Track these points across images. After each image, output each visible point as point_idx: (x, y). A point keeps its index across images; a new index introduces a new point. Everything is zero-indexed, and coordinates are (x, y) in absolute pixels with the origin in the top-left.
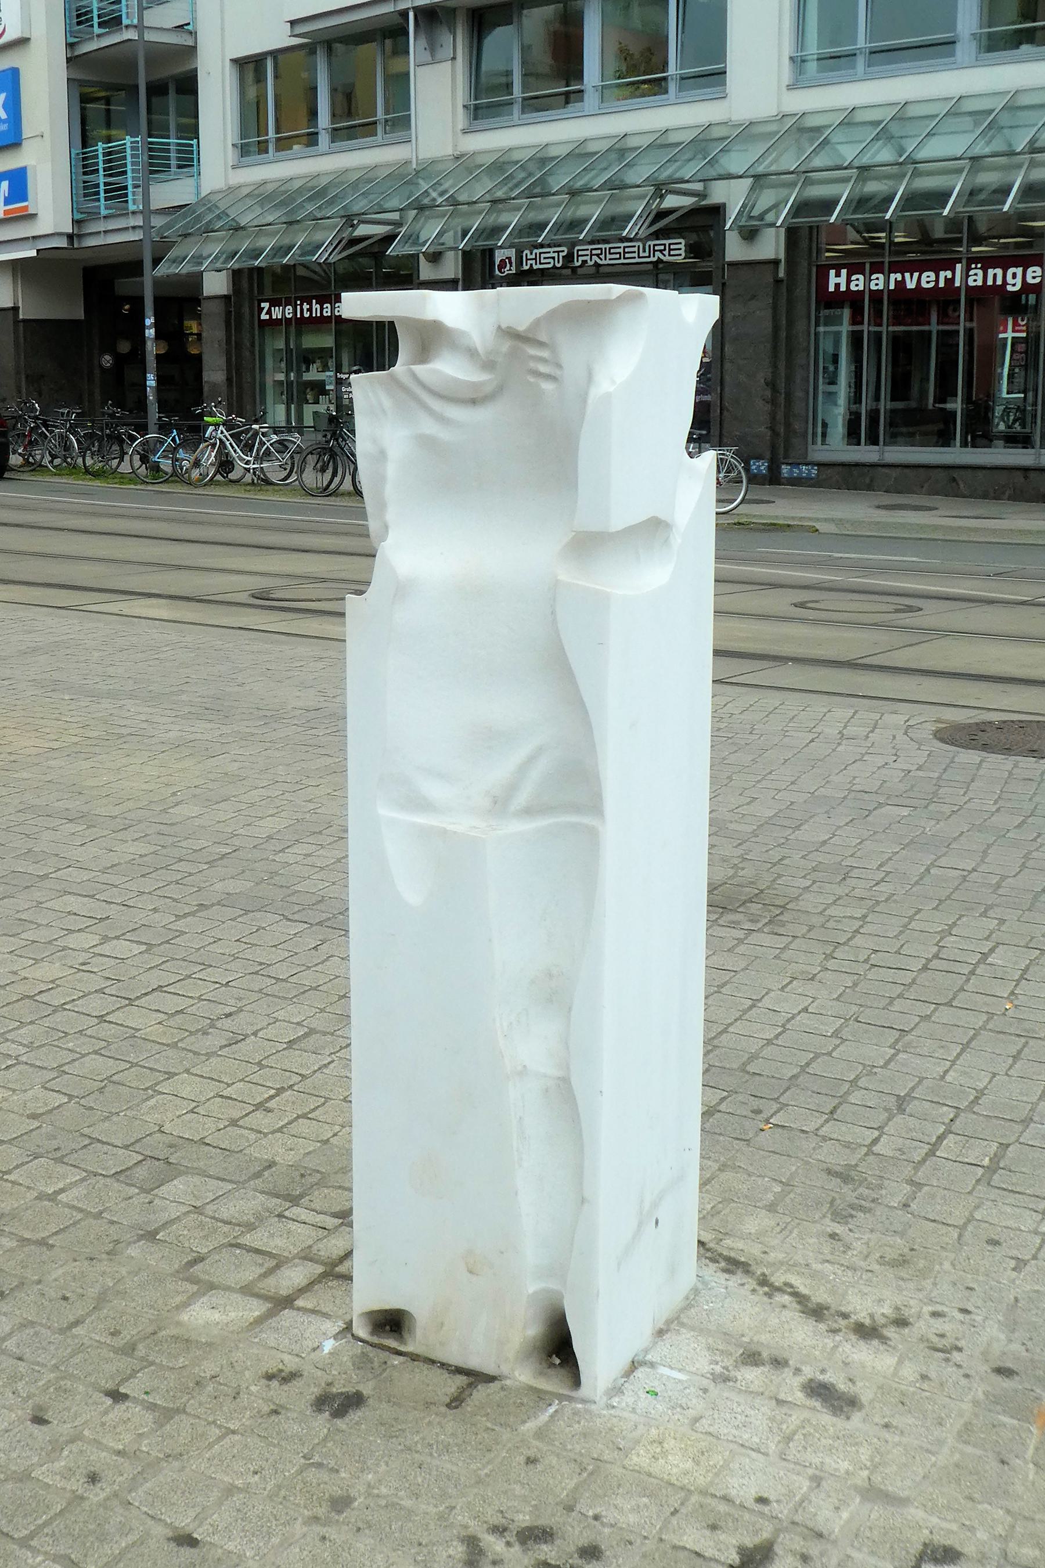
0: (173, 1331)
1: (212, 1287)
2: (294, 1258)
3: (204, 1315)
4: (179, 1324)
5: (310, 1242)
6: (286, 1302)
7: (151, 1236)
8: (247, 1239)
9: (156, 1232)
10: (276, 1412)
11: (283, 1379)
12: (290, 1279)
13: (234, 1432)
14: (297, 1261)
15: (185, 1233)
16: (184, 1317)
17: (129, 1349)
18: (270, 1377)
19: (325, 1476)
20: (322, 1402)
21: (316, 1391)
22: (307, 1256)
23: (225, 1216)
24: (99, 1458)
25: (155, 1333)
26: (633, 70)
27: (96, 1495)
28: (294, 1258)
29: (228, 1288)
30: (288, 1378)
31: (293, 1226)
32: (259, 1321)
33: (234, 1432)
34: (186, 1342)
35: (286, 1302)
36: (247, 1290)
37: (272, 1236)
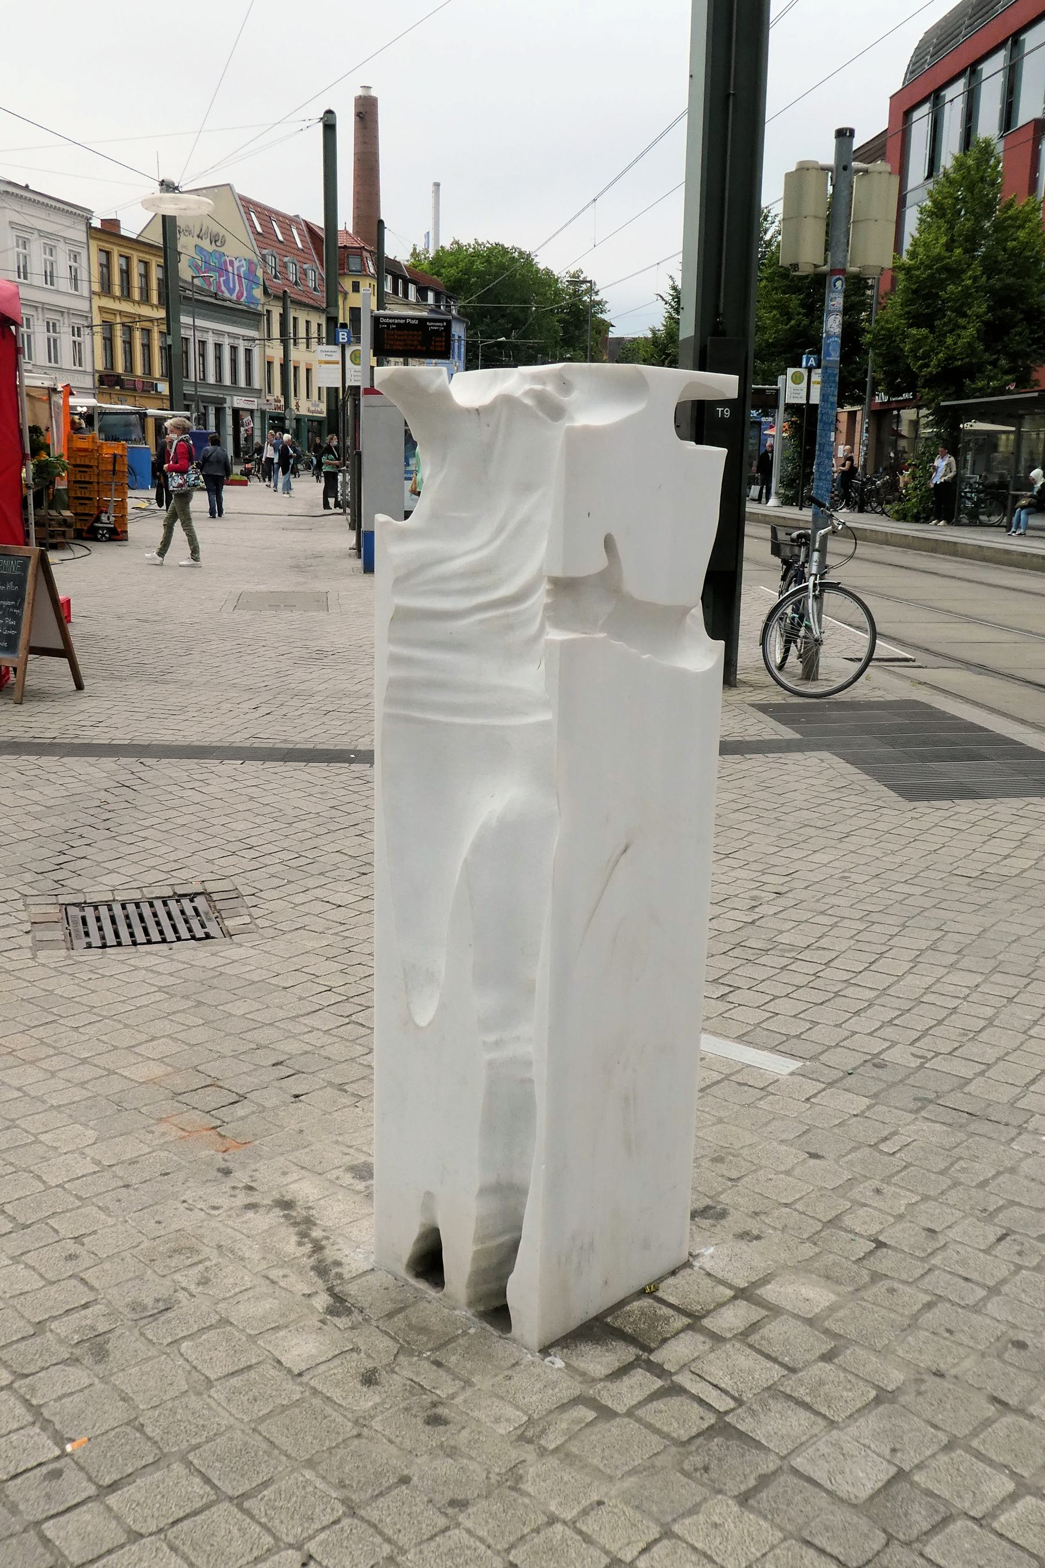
0: (841, 1289)
1: (810, 1322)
2: (730, 1339)
3: (816, 1296)
4: (838, 1294)
5: (712, 1356)
6: (742, 1294)
7: (883, 1397)
8: (777, 1372)
9: (878, 1401)
10: (756, 1213)
11: (748, 1234)
12: (736, 1316)
13: (786, 1205)
14: (729, 1335)
15: (845, 1394)
16: (833, 1297)
17: (876, 1277)
18: (758, 1238)
19: (725, 1173)
20: (723, 1214)
21: (723, 1222)
22: (717, 1339)
23: (804, 1415)
24: (876, 1202)
25: (856, 1290)
26: (1005, 507)
27: (876, 1183)
28: (730, 1339)
29: (796, 1316)
30: (744, 1236)
31: (726, 1383)
32: (765, 1280)
33: (786, 1205)
34: (828, 1277)
35: (742, 1294)
36: (774, 1311)
37: (751, 1372)
